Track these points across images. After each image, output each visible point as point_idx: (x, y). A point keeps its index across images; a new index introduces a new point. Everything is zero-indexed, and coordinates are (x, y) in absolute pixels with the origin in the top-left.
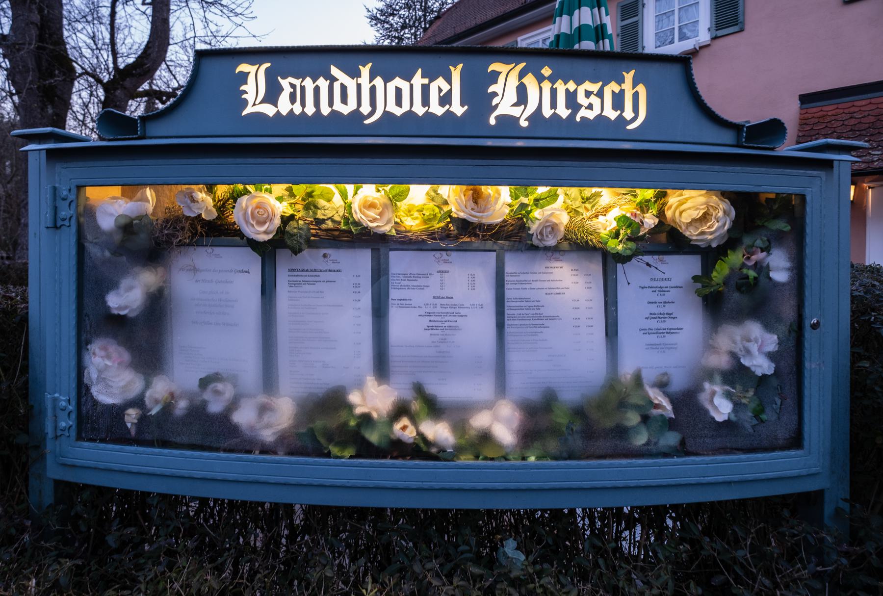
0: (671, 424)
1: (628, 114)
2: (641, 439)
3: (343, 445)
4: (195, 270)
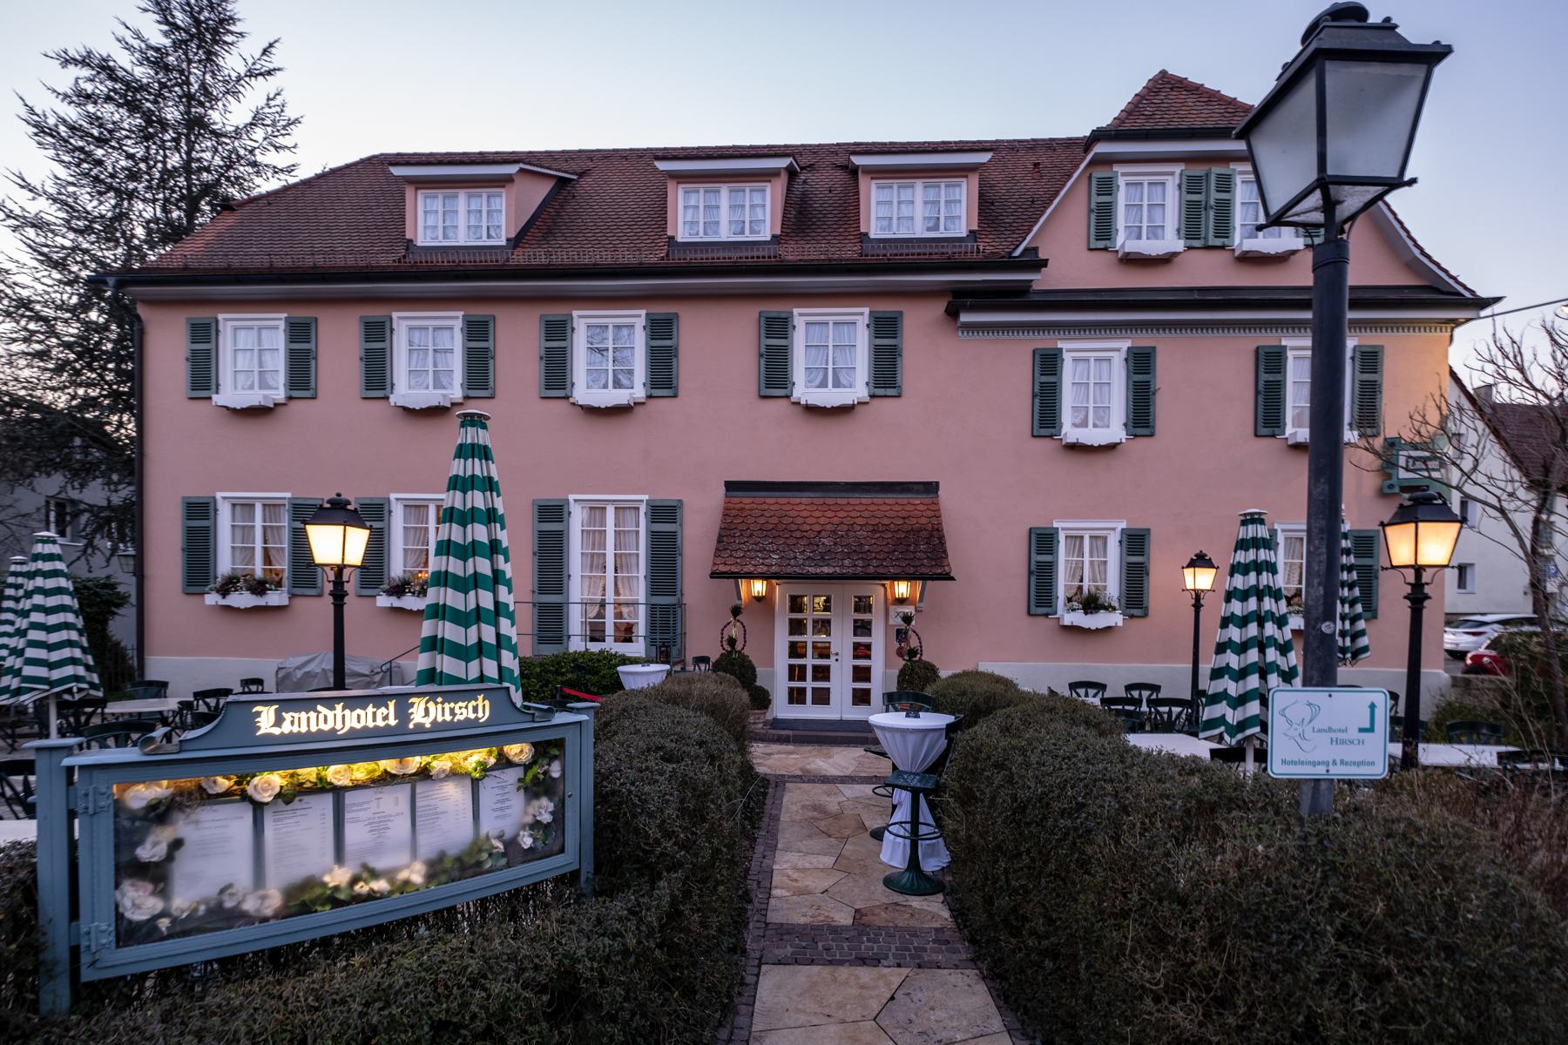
0: (504, 855)
1: (480, 714)
2: (487, 866)
3: (323, 905)
4: (197, 822)
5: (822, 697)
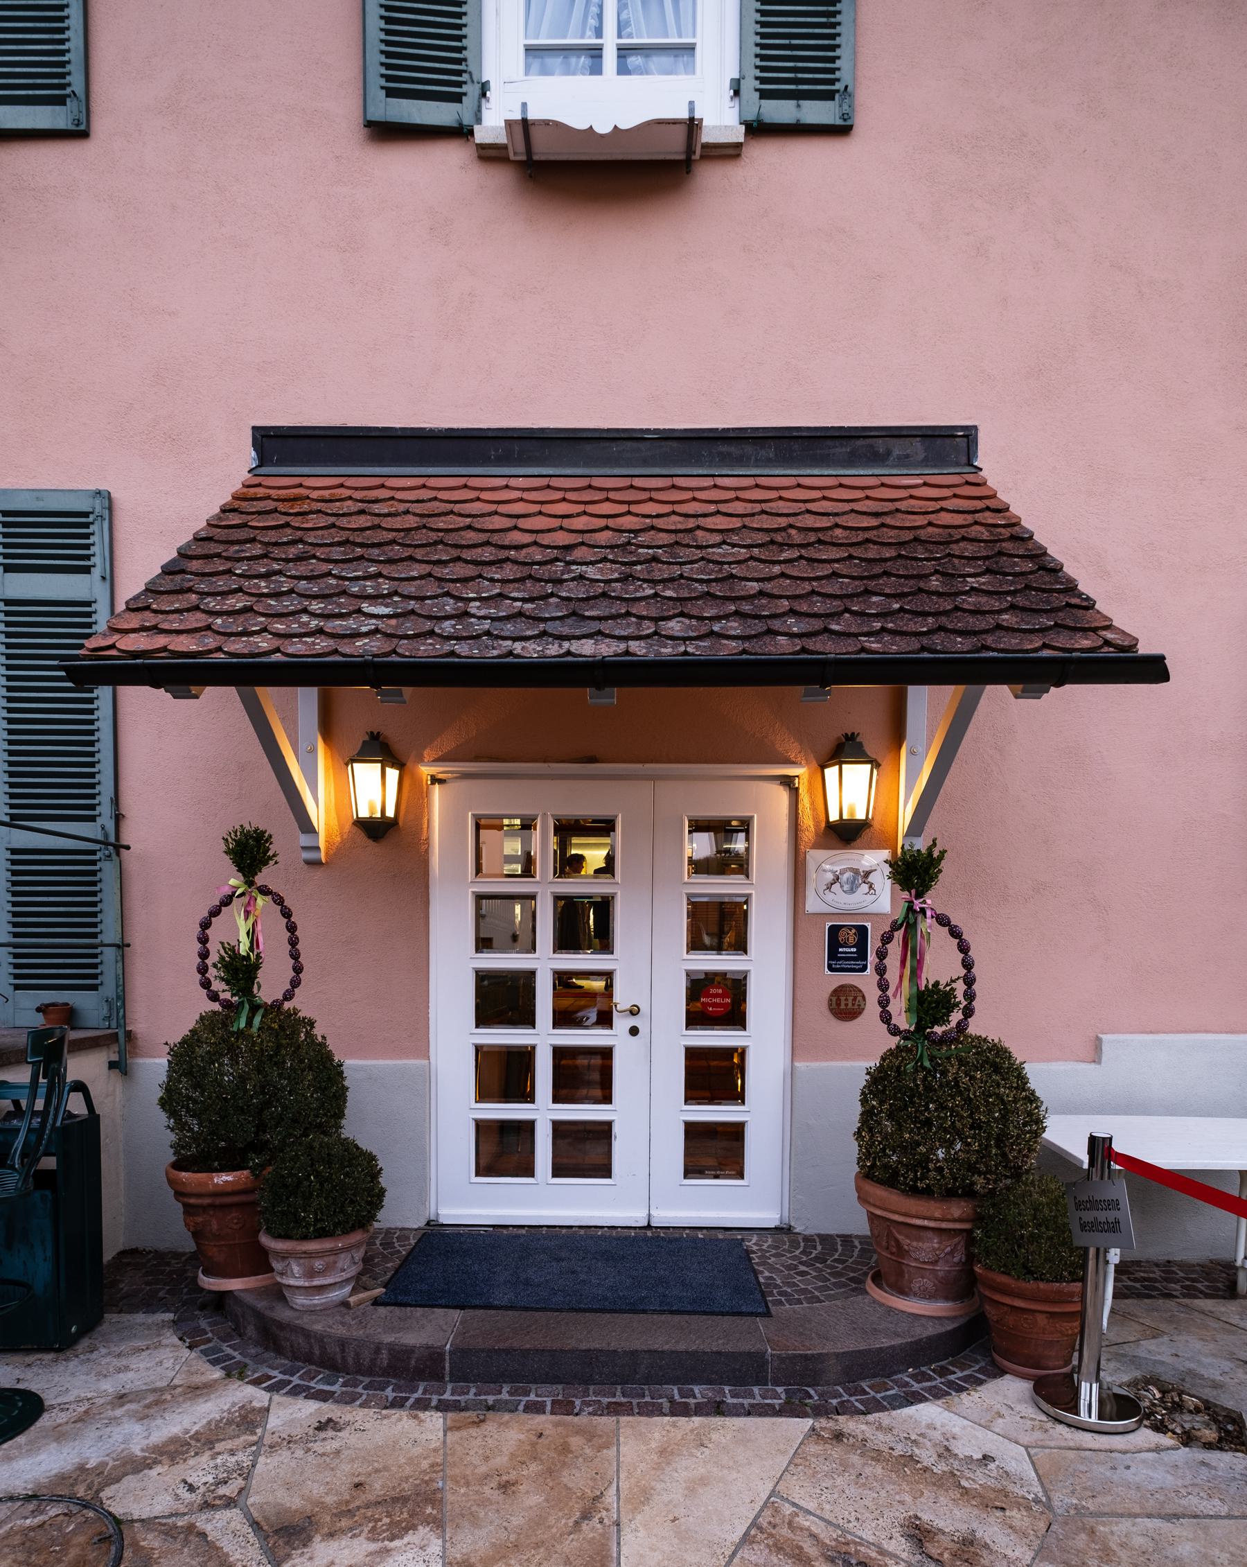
5: (585, 1152)
